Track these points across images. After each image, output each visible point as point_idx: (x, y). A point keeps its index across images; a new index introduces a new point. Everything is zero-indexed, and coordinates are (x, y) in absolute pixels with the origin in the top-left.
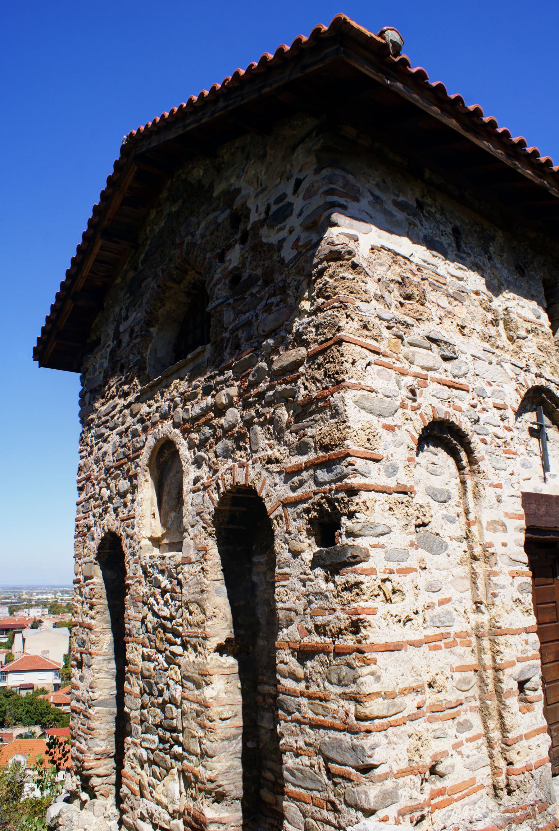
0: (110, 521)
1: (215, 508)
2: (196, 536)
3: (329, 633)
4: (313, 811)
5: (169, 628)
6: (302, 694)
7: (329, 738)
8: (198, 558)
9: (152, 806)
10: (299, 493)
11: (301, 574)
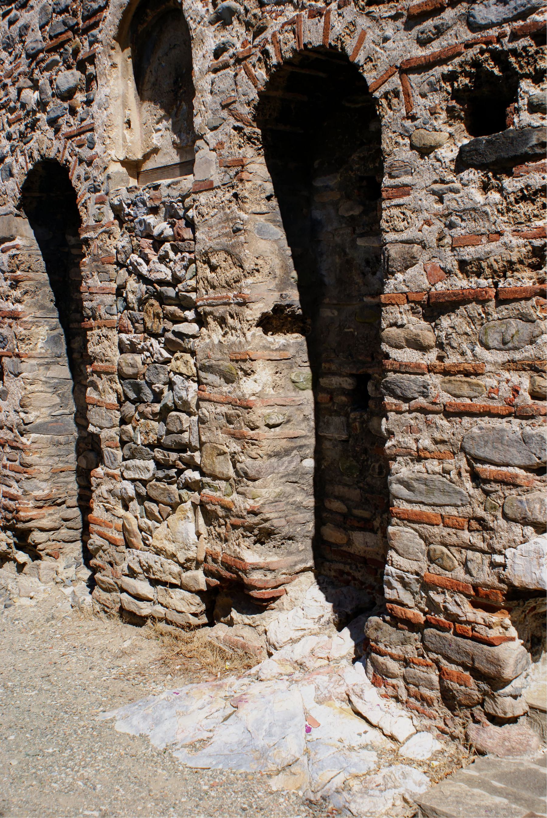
0: (45, 142)
1: (259, 94)
2: (221, 144)
3: (487, 271)
4: (444, 534)
5: (170, 298)
6: (431, 369)
7: (481, 429)
8: (227, 179)
9: (148, 557)
10: (435, 47)
11: (435, 182)
